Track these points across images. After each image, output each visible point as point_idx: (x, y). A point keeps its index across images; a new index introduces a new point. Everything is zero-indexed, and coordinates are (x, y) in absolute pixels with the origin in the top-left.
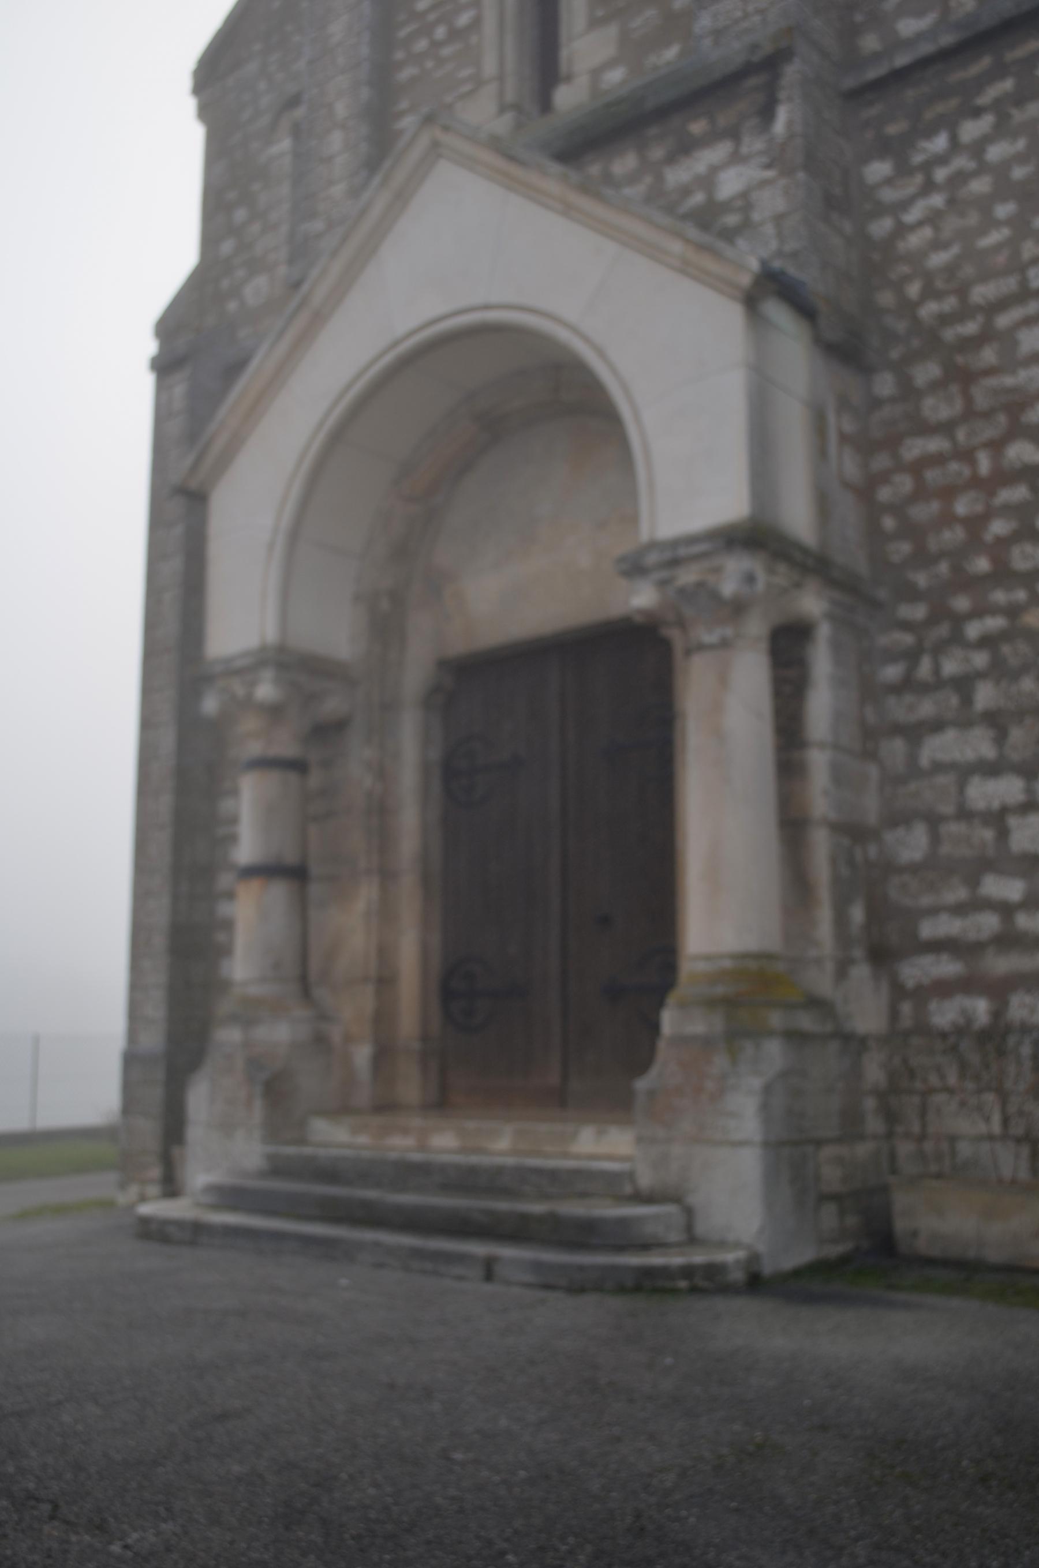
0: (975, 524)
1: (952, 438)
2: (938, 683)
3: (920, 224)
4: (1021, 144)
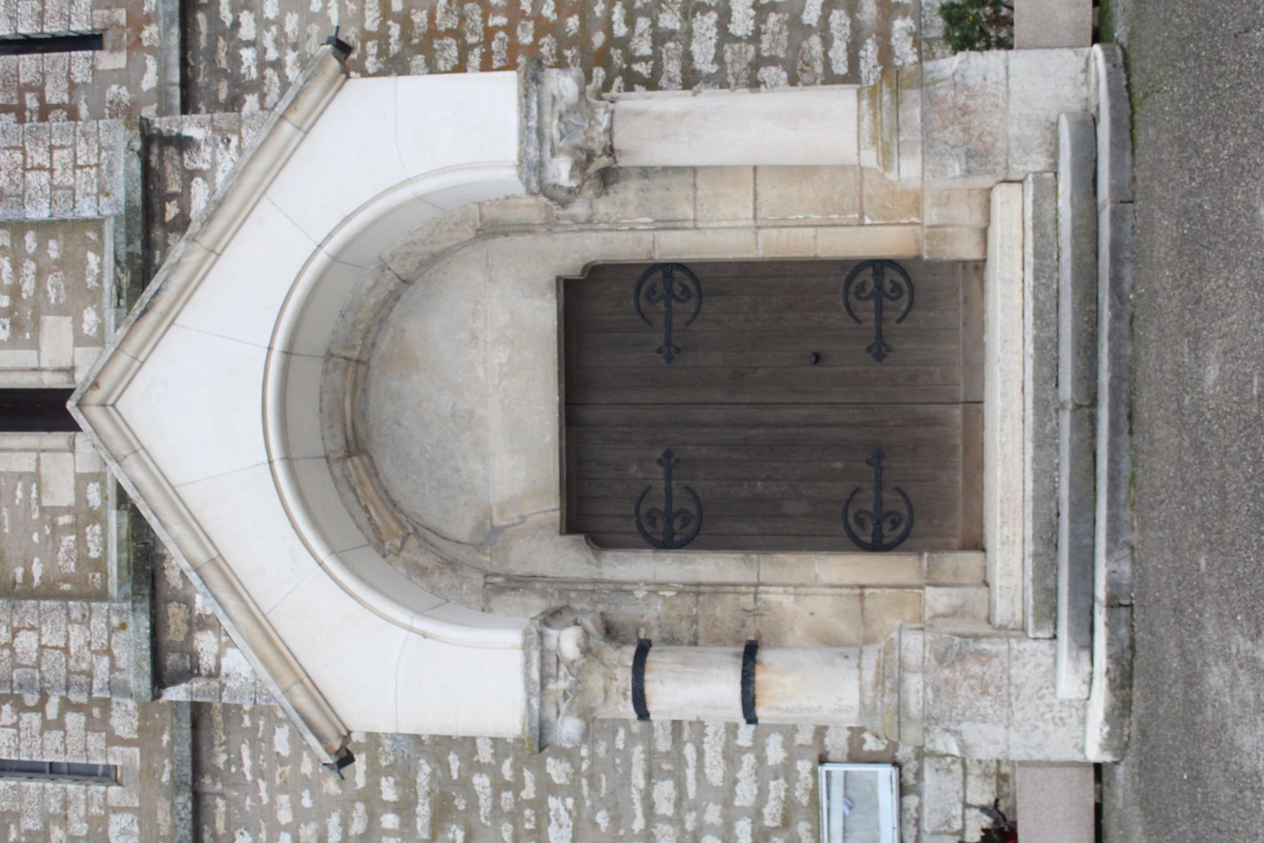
2: (656, 59)
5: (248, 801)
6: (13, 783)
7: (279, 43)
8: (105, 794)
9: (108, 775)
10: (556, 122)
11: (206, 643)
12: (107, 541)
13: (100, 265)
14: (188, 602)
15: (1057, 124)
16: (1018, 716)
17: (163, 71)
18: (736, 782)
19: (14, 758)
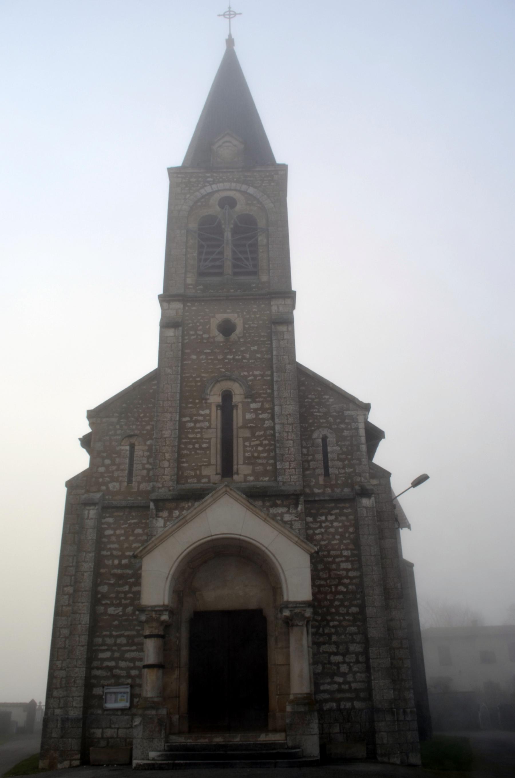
0: (332, 601)
1: (326, 582)
3: (319, 534)
4: (341, 524)
5: (122, 522)
6: (128, 455)
7: (327, 527)
8: (124, 481)
9: (130, 481)
10: (299, 611)
11: (165, 514)
12: (192, 484)
13: (265, 481)
14: (176, 509)
15: (299, 748)
16: (145, 741)
17: (318, 495)
18: (126, 661)
19: (135, 456)
